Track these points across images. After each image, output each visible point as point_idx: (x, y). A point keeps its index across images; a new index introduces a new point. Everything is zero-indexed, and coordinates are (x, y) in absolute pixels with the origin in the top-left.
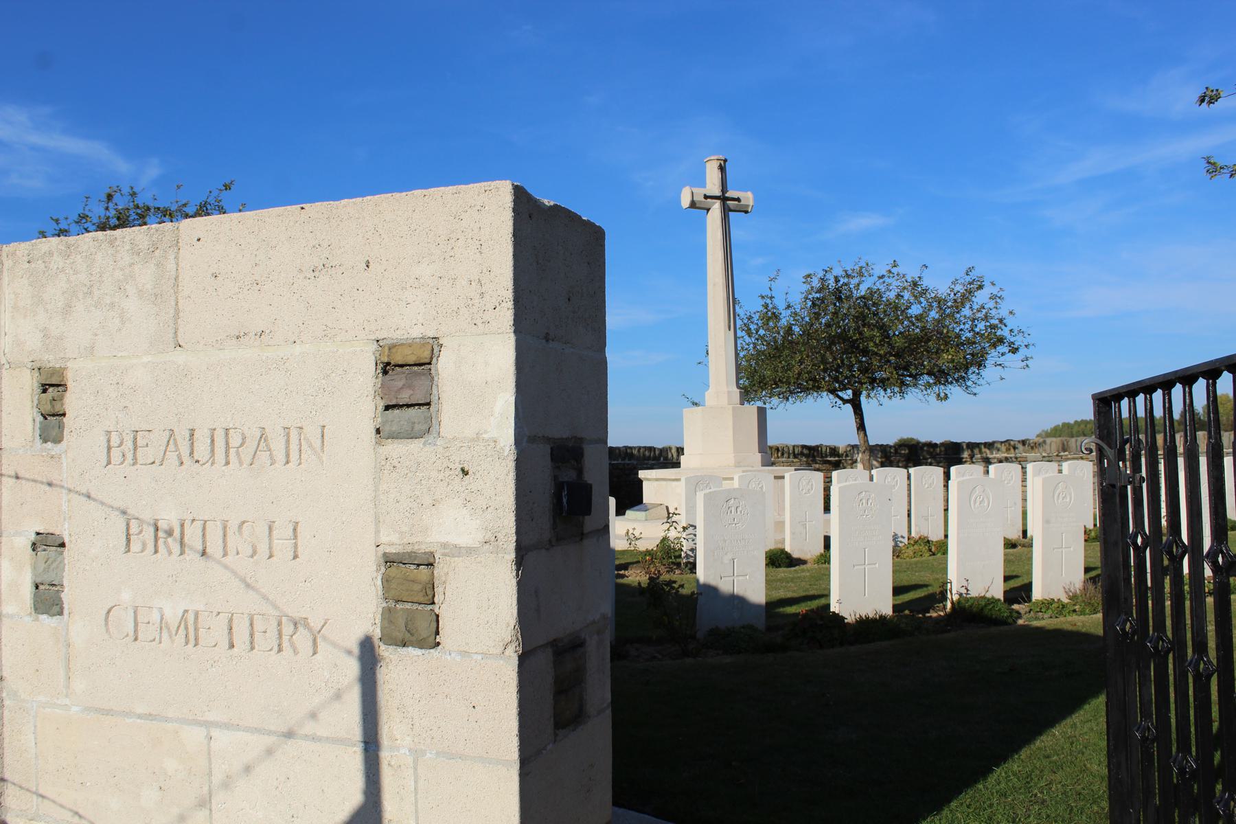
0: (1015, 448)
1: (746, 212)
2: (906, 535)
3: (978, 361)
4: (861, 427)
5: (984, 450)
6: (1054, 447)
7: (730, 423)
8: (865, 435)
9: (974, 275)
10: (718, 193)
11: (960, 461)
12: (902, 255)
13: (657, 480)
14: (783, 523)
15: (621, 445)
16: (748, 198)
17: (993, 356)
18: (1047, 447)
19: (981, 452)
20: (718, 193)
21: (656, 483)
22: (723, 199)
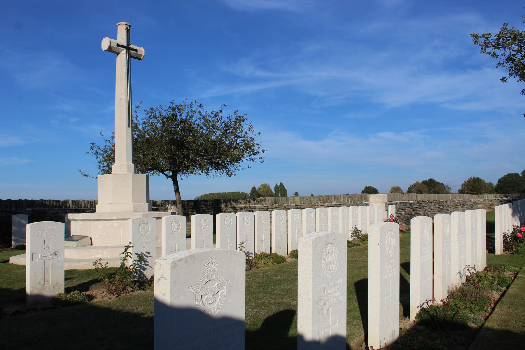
0: (249, 202)
1: (139, 59)
3: (238, 159)
4: (177, 191)
5: (232, 203)
6: (270, 202)
7: (131, 185)
9: (238, 114)
10: (124, 43)
11: (220, 211)
12: (206, 99)
13: (82, 220)
14: (161, 247)
15: (38, 199)
16: (142, 51)
18: (266, 202)
19: (231, 204)
20: (124, 43)
21: (81, 222)
22: (128, 48)
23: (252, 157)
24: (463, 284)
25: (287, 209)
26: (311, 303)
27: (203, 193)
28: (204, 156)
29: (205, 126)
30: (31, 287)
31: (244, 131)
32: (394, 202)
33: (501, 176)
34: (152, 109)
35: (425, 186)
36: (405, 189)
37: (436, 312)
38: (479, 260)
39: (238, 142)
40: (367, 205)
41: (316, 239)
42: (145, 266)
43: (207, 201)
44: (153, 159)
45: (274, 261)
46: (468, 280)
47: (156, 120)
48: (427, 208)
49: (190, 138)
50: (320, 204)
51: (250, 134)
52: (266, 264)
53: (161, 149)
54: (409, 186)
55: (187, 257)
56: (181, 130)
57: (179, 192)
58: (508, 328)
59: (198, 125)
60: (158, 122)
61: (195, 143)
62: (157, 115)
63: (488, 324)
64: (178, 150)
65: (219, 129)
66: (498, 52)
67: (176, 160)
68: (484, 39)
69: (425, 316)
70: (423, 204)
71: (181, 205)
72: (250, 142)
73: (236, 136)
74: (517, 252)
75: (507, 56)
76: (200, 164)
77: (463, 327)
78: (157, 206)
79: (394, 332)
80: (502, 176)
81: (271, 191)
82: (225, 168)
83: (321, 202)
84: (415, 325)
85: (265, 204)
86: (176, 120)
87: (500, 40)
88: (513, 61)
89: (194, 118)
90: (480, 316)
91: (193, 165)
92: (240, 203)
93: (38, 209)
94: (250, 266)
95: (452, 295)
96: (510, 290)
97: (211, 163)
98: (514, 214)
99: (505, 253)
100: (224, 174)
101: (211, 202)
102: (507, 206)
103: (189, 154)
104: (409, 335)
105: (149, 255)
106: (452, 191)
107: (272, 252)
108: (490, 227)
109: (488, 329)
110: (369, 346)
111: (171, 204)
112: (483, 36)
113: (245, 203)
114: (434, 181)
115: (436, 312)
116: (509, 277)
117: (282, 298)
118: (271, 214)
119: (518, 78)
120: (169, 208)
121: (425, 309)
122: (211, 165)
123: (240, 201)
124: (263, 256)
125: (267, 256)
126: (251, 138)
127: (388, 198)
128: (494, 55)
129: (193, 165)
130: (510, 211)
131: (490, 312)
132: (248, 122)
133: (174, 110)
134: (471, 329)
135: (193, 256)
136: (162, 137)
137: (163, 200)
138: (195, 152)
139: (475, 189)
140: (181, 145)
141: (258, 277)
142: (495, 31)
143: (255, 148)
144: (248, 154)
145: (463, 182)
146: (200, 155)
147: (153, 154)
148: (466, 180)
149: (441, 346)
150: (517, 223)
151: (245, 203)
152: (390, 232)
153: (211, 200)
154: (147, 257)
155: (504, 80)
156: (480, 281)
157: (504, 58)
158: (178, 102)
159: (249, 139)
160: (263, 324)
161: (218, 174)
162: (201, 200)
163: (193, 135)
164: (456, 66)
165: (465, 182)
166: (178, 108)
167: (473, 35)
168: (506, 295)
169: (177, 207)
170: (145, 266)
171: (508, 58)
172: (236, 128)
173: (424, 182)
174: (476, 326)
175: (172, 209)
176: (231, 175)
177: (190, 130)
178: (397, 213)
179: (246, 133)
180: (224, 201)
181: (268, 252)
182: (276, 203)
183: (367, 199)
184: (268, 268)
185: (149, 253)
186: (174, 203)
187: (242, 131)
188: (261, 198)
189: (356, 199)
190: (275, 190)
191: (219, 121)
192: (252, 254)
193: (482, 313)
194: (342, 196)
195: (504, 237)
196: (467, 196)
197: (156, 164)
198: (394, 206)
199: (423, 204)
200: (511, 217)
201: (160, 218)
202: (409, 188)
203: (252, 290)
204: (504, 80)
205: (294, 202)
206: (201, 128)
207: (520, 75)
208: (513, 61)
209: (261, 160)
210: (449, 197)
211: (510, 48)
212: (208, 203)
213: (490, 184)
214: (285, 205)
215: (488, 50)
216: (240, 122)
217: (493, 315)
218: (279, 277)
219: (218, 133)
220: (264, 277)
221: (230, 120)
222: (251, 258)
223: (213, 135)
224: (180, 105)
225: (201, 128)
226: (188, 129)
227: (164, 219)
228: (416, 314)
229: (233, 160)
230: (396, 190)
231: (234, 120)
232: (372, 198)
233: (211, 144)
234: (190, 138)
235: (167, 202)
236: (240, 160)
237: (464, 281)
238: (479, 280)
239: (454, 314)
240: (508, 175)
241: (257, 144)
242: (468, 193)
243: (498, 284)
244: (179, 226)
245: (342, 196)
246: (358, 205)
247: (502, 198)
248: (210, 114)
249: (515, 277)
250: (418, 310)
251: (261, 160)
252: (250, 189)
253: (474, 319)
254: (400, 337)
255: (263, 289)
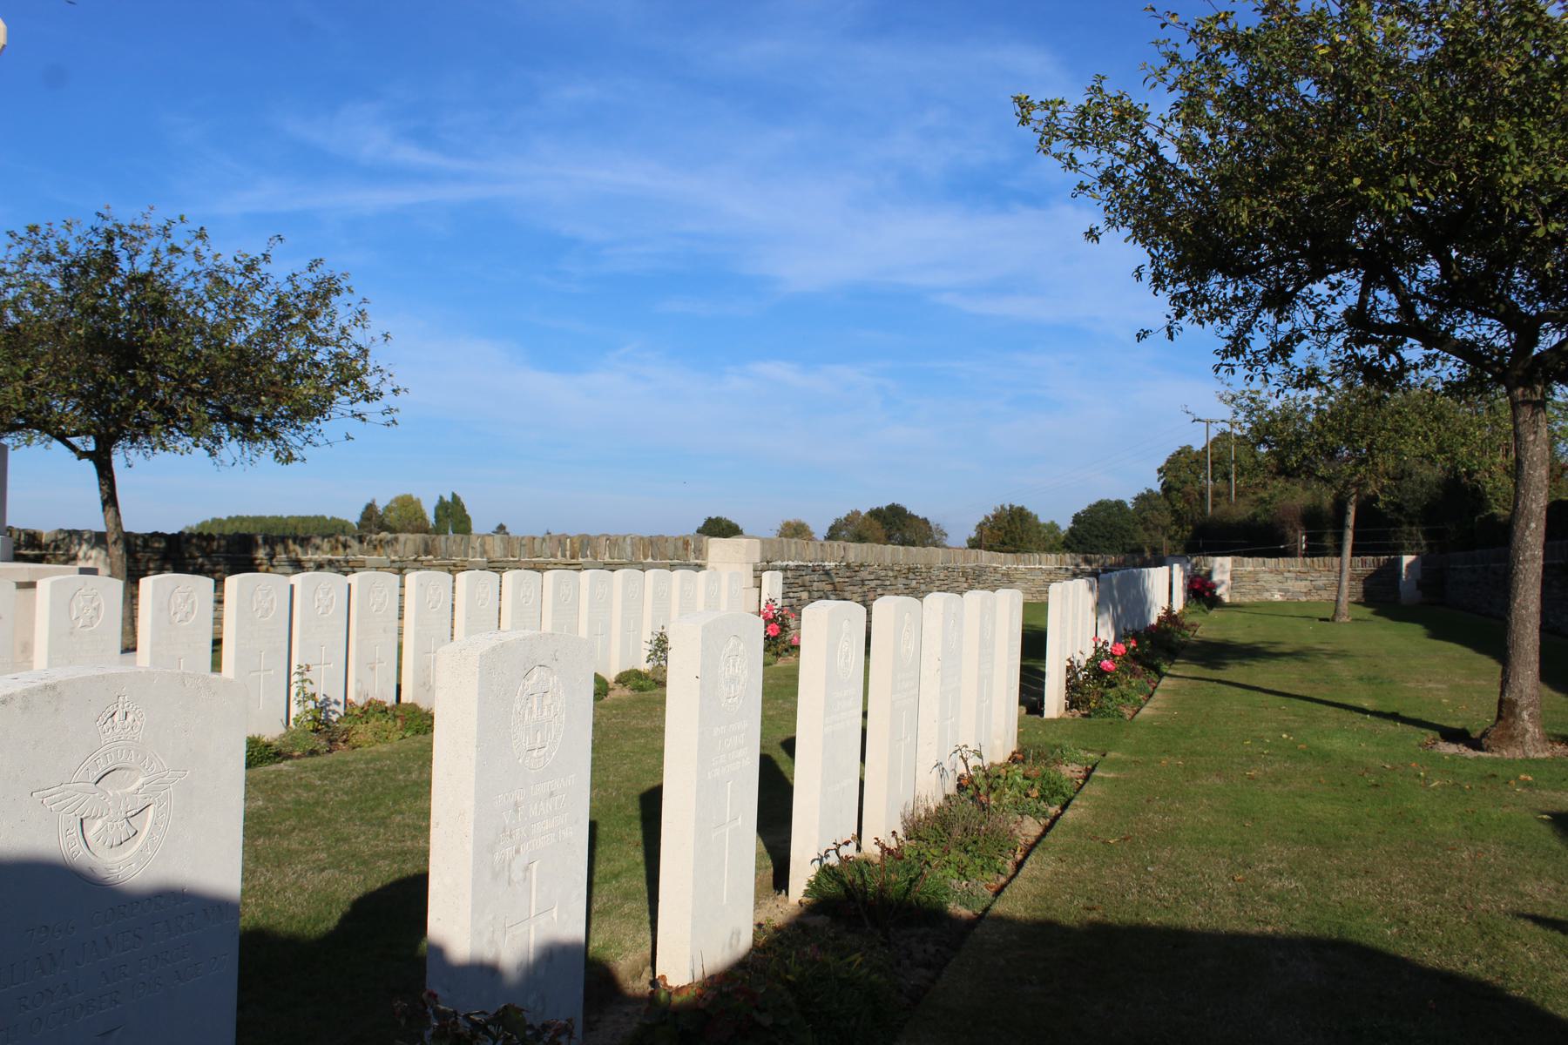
0: (345, 546)
2: (342, 700)
3: (315, 409)
6: (410, 547)
8: (118, 514)
9: (322, 272)
11: (250, 566)
17: (342, 403)
18: (399, 547)
19: (287, 550)
23: (361, 406)
24: (947, 797)
25: (453, 569)
26: (469, 847)
27: (207, 516)
28: (203, 394)
29: (211, 299)
31: (337, 325)
32: (779, 563)
33: (1081, 506)
34: (33, 229)
35: (877, 524)
36: (820, 529)
37: (862, 875)
38: (995, 731)
39: (318, 358)
40: (699, 567)
41: (494, 649)
43: (210, 538)
44: (29, 394)
45: (404, 728)
46: (960, 787)
47: (46, 269)
48: (873, 584)
49: (158, 336)
50: (564, 561)
51: (358, 336)
52: (379, 737)
53: (56, 361)
54: (831, 522)
55: (30, 692)
56: (130, 308)
57: (115, 504)
58: (1050, 915)
59: (190, 294)
60: (53, 274)
61: (176, 351)
62: (54, 251)
63: (999, 908)
64: (120, 370)
65: (257, 313)
66: (1082, 155)
67: (108, 400)
68: (1048, 113)
69: (831, 888)
70: (864, 574)
71: (120, 546)
72: (355, 359)
73: (311, 339)
74: (1100, 711)
75: (1102, 168)
76: (190, 420)
77: (934, 916)
78: (40, 547)
79: (737, 934)
80: (1085, 507)
81: (423, 517)
82: (273, 436)
83: (564, 556)
84: (801, 915)
85: (396, 553)
86: (113, 273)
87: (1088, 123)
88: (1118, 185)
89: (175, 270)
90: (981, 885)
91: (166, 421)
92: (318, 548)
94: (331, 741)
95: (914, 829)
96: (1068, 814)
97: (227, 417)
98: (1100, 606)
99: (1068, 715)
100: (267, 449)
101: (223, 542)
102: (1082, 584)
103: (154, 384)
104: (781, 943)
106: (948, 543)
107: (403, 700)
108: (1034, 644)
109: (1000, 920)
110: (658, 974)
111: (88, 541)
112: (1045, 105)
113: (334, 549)
114: (904, 510)
115: (862, 875)
116: (1071, 780)
117: (414, 837)
118: (402, 586)
119: (1126, 231)
120: (81, 554)
121: (831, 868)
122: (229, 426)
123: (318, 541)
124: (373, 709)
125: (385, 711)
126: (360, 348)
127: (763, 551)
128: (1072, 163)
129: (166, 421)
130: (1089, 599)
131: (1010, 873)
132: (354, 300)
133: (110, 240)
134: (955, 921)
135: (53, 687)
136: (61, 323)
137: (61, 531)
138: (172, 377)
139: (1013, 539)
140: (128, 355)
141: (350, 774)
142: (1078, 98)
143: (371, 381)
144: (347, 398)
145: (982, 519)
146: (190, 390)
147: (28, 377)
148: (991, 512)
149: (865, 971)
150: (1107, 634)
151: (334, 549)
152: (733, 641)
153: (222, 536)
155: (1092, 234)
156: (991, 788)
157: (1096, 173)
158: (125, 215)
159: (352, 352)
160: (346, 919)
161: (247, 454)
162: (191, 535)
163: (173, 325)
164: (980, 189)
166: (123, 235)
167: (1018, 99)
168: (1057, 825)
169: (108, 555)
171: (1106, 172)
172: (311, 315)
173: (876, 514)
174: (970, 913)
175: (93, 557)
176: (290, 458)
177: (159, 309)
178: (785, 596)
179: (343, 330)
180: (266, 541)
181: (390, 700)
182: (427, 553)
183: (700, 552)
184: (384, 748)
186: (99, 540)
187: (331, 324)
188: (383, 535)
189: (670, 551)
190: (436, 516)
191: (257, 286)
192: (337, 703)
193: (992, 876)
194: (628, 540)
195: (1068, 669)
196: (985, 557)
197: (39, 411)
198: (780, 574)
199: (864, 574)
200: (1091, 616)
201: (32, 585)
202: (831, 529)
203: (325, 812)
204: (1092, 234)
205: (484, 552)
206: (200, 304)
207: (1135, 228)
208: (1118, 185)
209: (388, 418)
210: (936, 556)
211: (1111, 149)
212: (215, 544)
213: (1053, 527)
214: (456, 559)
215: (1059, 146)
216: (326, 296)
217: (1016, 882)
218: (414, 776)
219: (254, 324)
220: (367, 775)
221: (296, 287)
222: (334, 718)
223: (237, 330)
224: (132, 227)
225: (200, 304)
226: (153, 306)
227: (44, 585)
228: (805, 882)
229: (297, 413)
230: (796, 530)
231: (307, 287)
232: (717, 547)
233: (228, 358)
234: (158, 336)
235: (75, 535)
236: (322, 413)
237: (951, 789)
238: (990, 787)
239: (911, 881)
240: (1100, 503)
241: (378, 369)
242: (990, 548)
243: (1042, 797)
244: (97, 609)
245: (628, 540)
246: (672, 567)
247: (1077, 565)
248: (230, 263)
249: (1086, 779)
250: (812, 871)
251: (388, 418)
252: (360, 509)
253: (963, 893)
254: (756, 948)
255: (360, 810)
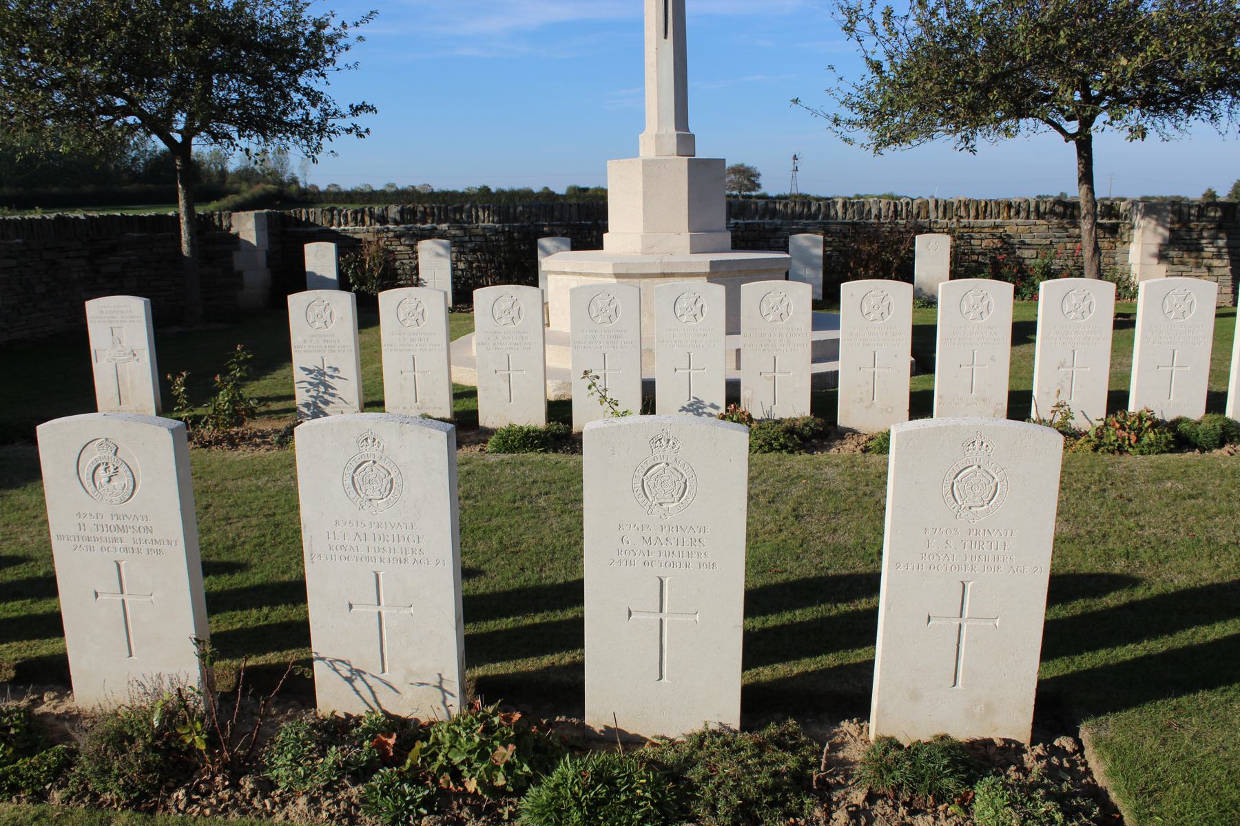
4: (1086, 177)
30: (1137, 402)
42: (326, 397)
93: (757, 220)
100: (904, 145)
105: (336, 374)
154: (332, 377)
165: (1211, 195)
170: (326, 397)
174: (1135, 270)
185: (336, 369)
